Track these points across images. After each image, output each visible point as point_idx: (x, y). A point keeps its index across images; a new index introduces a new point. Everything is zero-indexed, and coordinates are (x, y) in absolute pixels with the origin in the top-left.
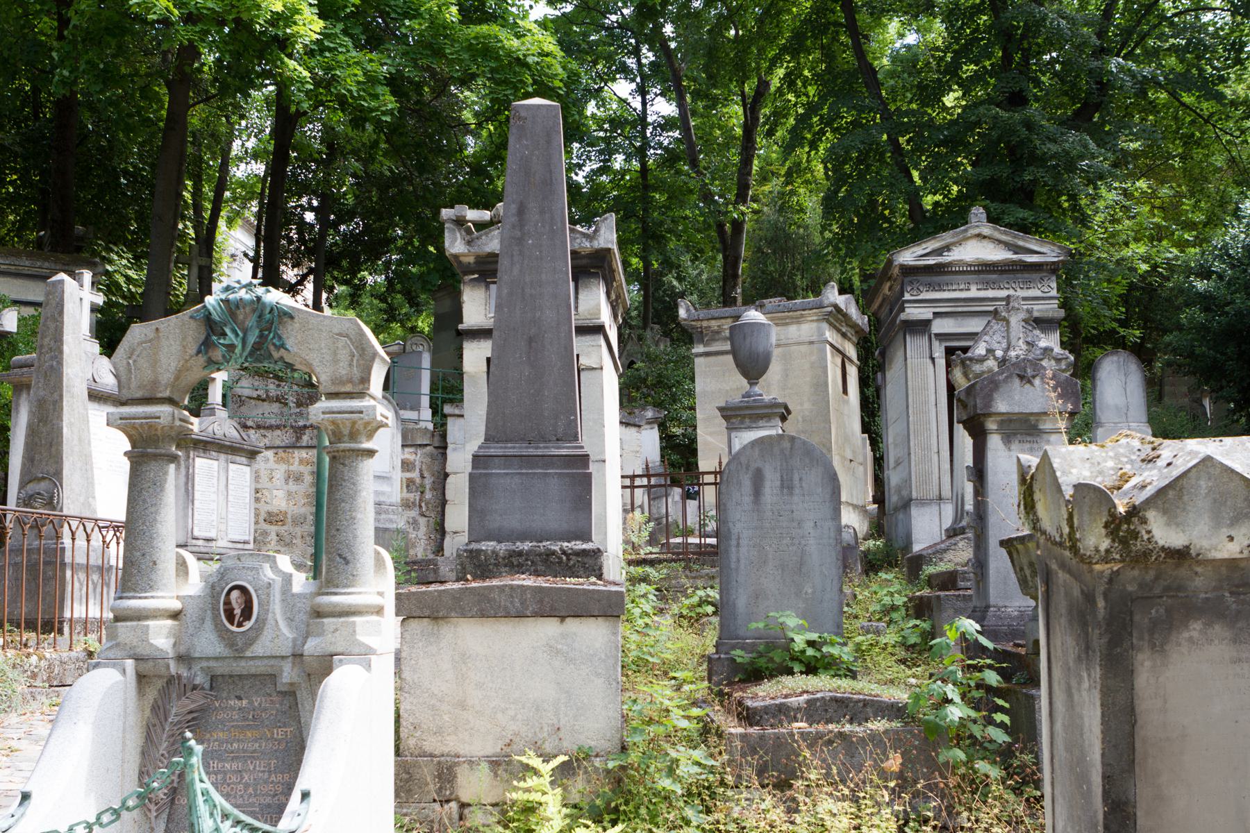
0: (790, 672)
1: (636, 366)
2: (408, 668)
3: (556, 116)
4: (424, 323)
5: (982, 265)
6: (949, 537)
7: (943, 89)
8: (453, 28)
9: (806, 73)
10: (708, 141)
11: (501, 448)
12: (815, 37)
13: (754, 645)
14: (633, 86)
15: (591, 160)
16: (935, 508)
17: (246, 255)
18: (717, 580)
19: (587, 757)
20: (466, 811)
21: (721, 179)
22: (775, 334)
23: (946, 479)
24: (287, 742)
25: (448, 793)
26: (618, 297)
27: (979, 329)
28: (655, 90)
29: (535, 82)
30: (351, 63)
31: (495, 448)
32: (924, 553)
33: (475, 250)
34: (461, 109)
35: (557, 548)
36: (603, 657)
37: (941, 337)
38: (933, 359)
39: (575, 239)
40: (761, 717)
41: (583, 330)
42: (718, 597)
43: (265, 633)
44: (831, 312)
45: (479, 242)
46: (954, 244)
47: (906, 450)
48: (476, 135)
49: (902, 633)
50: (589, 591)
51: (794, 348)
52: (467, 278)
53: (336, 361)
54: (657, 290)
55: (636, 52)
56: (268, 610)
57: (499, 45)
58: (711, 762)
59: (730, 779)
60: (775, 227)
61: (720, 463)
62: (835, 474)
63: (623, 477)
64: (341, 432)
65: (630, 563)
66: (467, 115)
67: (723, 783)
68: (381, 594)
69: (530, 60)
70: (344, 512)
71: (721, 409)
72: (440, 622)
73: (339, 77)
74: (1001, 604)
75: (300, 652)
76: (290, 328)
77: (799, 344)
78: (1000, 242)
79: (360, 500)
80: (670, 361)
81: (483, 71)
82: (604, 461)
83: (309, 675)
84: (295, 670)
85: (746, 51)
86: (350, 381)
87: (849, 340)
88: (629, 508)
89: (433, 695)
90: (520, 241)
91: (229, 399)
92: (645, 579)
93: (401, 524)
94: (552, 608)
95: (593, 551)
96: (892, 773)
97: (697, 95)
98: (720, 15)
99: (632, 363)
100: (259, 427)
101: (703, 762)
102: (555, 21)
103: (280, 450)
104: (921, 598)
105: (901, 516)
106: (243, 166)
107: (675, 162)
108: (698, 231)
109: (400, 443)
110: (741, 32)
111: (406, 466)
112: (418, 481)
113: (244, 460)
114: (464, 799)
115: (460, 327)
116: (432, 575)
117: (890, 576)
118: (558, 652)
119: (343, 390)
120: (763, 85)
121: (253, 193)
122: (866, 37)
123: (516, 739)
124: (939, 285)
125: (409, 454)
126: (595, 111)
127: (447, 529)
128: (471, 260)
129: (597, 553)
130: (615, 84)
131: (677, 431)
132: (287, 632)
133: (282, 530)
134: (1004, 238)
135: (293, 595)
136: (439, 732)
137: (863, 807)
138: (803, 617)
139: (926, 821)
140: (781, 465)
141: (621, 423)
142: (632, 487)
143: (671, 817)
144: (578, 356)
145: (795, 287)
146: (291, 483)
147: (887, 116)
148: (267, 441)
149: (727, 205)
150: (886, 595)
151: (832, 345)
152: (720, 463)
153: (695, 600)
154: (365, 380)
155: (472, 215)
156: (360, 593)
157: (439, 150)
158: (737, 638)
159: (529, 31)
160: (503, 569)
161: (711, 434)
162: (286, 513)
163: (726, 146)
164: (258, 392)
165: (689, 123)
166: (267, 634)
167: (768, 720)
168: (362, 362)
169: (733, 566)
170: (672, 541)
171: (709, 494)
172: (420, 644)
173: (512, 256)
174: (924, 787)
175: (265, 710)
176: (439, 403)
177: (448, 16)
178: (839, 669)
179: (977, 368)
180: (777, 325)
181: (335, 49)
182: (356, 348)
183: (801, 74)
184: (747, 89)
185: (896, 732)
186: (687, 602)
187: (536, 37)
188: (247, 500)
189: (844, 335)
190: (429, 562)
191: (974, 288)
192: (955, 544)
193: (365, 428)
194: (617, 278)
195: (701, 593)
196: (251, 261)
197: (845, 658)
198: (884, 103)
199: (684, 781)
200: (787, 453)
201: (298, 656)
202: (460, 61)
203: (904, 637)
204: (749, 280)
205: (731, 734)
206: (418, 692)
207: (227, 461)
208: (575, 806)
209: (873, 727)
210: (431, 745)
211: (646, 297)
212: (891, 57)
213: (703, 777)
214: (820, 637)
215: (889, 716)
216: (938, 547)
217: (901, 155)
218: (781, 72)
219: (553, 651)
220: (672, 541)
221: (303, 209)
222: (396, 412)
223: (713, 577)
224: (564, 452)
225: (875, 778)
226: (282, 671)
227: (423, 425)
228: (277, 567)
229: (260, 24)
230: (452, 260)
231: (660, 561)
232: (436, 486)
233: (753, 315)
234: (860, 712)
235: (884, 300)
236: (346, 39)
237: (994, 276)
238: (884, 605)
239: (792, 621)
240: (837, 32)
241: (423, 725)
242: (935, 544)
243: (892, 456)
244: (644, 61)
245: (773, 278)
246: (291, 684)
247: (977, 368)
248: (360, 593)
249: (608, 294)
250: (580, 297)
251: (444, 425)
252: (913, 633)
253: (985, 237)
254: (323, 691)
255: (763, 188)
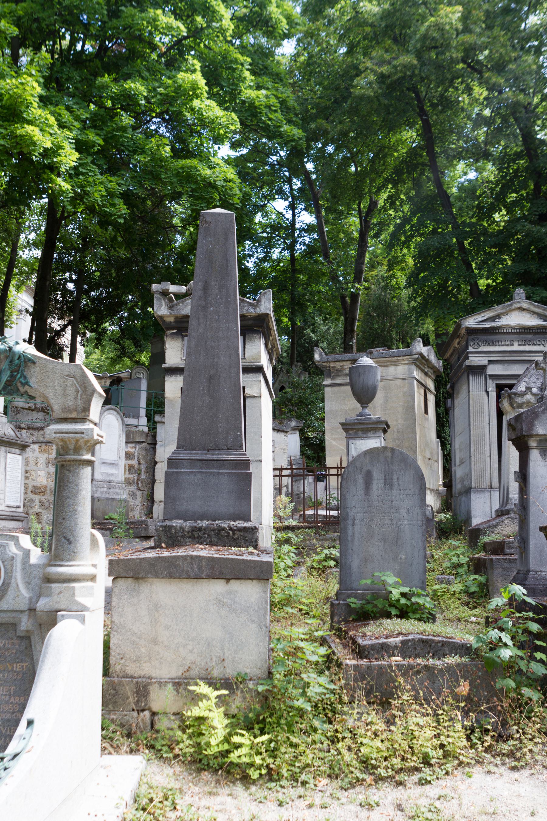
0: (389, 616)
1: (284, 391)
2: (116, 614)
3: (232, 221)
4: (144, 358)
5: (522, 329)
6: (498, 516)
7: (493, 208)
8: (167, 161)
9: (402, 196)
10: (335, 240)
11: (188, 454)
12: (409, 172)
13: (363, 594)
14: (287, 203)
15: (257, 252)
16: (487, 494)
17: (27, 311)
18: (338, 542)
19: (243, 681)
20: (156, 718)
21: (344, 266)
22: (380, 373)
23: (496, 474)
24: (23, 674)
25: (143, 704)
26: (273, 346)
27: (521, 372)
28: (301, 206)
29: (221, 199)
30: (97, 182)
31: (184, 454)
32: (481, 527)
33: (175, 313)
34: (172, 217)
35: (226, 526)
36: (256, 608)
37: (494, 377)
38: (487, 392)
39: (244, 306)
40: (369, 652)
41: (247, 370)
42: (338, 555)
43: (9, 593)
44: (418, 358)
45: (178, 307)
46: (503, 314)
47: (468, 454)
48: (182, 234)
49: (466, 584)
50: (247, 561)
51: (392, 382)
52: (169, 332)
53: (65, 395)
54: (300, 339)
55: (289, 181)
56: (11, 576)
57: (197, 173)
58: (332, 686)
59: (346, 699)
60: (379, 299)
61: (341, 461)
62: (423, 475)
63: (274, 469)
64: (68, 447)
65: (278, 529)
66: (176, 221)
67: (341, 701)
68: (94, 566)
69: (218, 183)
70: (69, 505)
71: (342, 424)
72: (140, 581)
73: (89, 192)
74: (538, 569)
75: (34, 607)
76: (33, 370)
77: (396, 379)
78: (534, 313)
79: (80, 497)
80: (308, 387)
81: (187, 191)
82: (261, 461)
83: (40, 625)
84: (31, 620)
85: (363, 181)
86: (75, 410)
87: (430, 377)
88: (278, 490)
89: (135, 633)
90: (205, 308)
91: (9, 409)
92: (287, 541)
93: (124, 496)
94: (221, 573)
95: (252, 528)
96: (462, 696)
97: (329, 210)
98: (344, 157)
99: (282, 388)
100: (29, 428)
101: (327, 686)
102: (237, 159)
103: (43, 444)
104: (479, 559)
105: (463, 498)
106: (27, 252)
107: (313, 255)
108: (329, 301)
109: (124, 441)
110: (359, 169)
111: (129, 456)
112: (136, 466)
113: (18, 451)
114: (155, 709)
115: (163, 366)
116: (144, 531)
117: (457, 543)
118: (224, 604)
119: (70, 416)
120: (373, 204)
121: (33, 269)
122: (443, 173)
123: (193, 667)
124: (493, 341)
125: (130, 448)
126: (261, 219)
127: (155, 499)
128: (172, 319)
129: (254, 530)
130: (274, 202)
131: (311, 434)
132: (25, 593)
133: (43, 498)
134: (537, 310)
135: (31, 565)
136: (138, 660)
137: (442, 721)
138: (398, 576)
139: (487, 731)
140: (385, 468)
141: (274, 429)
142: (281, 476)
143: (303, 726)
144: (244, 388)
145: (392, 338)
146: (50, 467)
147: (456, 226)
148: (34, 438)
149: (347, 283)
150: (454, 556)
151: (418, 381)
152: (341, 461)
153: (322, 556)
154: (86, 409)
155: (173, 289)
156: (79, 565)
157: (156, 244)
158: (352, 590)
159: (218, 164)
160: (188, 540)
161: (335, 439)
162: (46, 487)
163: (347, 244)
164: (29, 405)
165: (323, 229)
166: (11, 594)
167: (373, 655)
168: (84, 396)
169: (350, 538)
170: (307, 512)
171: (333, 481)
172: (126, 597)
173: (199, 318)
174: (486, 708)
175: (8, 649)
176: (152, 413)
177: (163, 152)
178: (423, 614)
179: (519, 400)
180: (380, 366)
181: (87, 173)
182: (80, 386)
183: (399, 198)
184: (362, 206)
185: (465, 665)
186: (317, 558)
187: (222, 169)
188: (19, 478)
189: (426, 374)
190: (142, 522)
191: (516, 344)
192: (502, 522)
193: (85, 444)
194: (273, 334)
195: (326, 551)
196: (30, 314)
197: (427, 605)
198: (454, 217)
199: (313, 699)
200: (389, 460)
201: (32, 610)
202: (171, 183)
203: (466, 586)
204: (361, 333)
205: (347, 665)
206: (123, 631)
207: (6, 452)
208: (234, 716)
209: (449, 662)
210: (132, 669)
211: (292, 343)
212: (458, 187)
213: (327, 696)
214: (410, 591)
215: (460, 653)
216: (491, 523)
217: (465, 253)
218: (385, 195)
219: (221, 603)
220: (307, 512)
221: (66, 281)
222: (122, 420)
223: (335, 540)
224: (232, 457)
225: (451, 701)
226: (20, 621)
227: (140, 428)
228: (19, 545)
229: (36, 156)
230: (159, 319)
231: (298, 528)
232: (149, 470)
233: (366, 360)
234: (440, 650)
235: (454, 351)
236: (94, 167)
237: (530, 336)
238: (453, 563)
239: (391, 579)
240: (424, 170)
241: (126, 655)
242: (489, 521)
243: (457, 456)
244: (295, 187)
245: (377, 333)
246: (27, 631)
247: (519, 400)
248: (79, 565)
249: (266, 345)
250: (247, 347)
251: (155, 428)
252: (473, 584)
253: (524, 310)
254: (48, 640)
255: (372, 273)
